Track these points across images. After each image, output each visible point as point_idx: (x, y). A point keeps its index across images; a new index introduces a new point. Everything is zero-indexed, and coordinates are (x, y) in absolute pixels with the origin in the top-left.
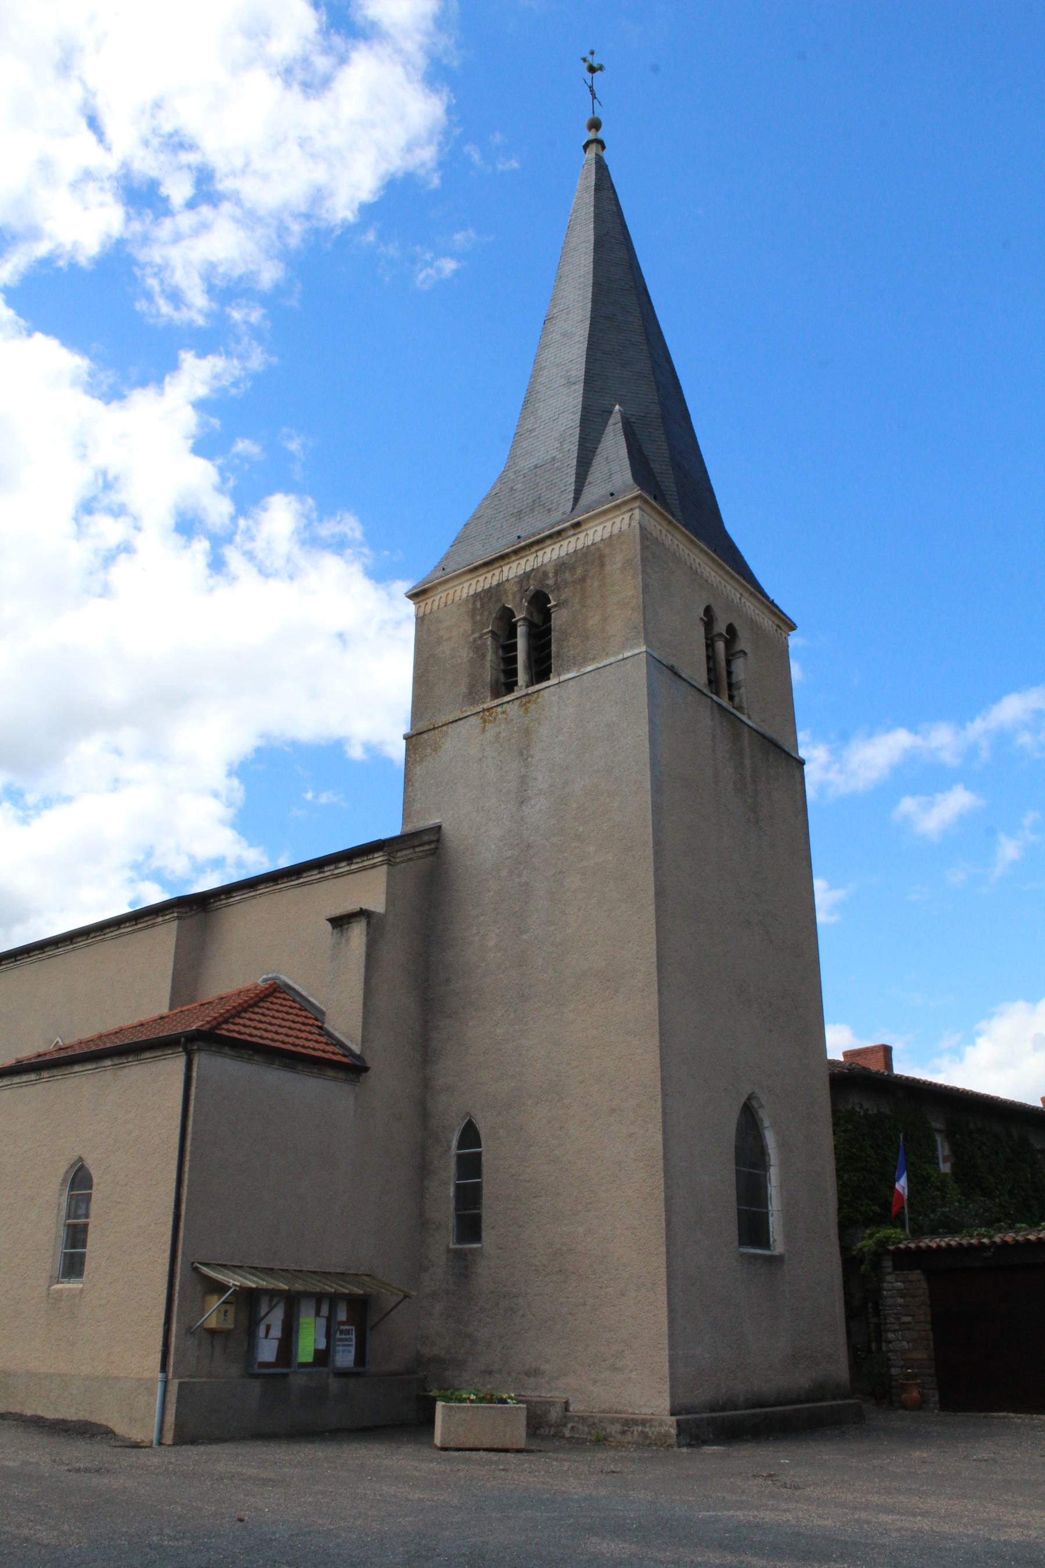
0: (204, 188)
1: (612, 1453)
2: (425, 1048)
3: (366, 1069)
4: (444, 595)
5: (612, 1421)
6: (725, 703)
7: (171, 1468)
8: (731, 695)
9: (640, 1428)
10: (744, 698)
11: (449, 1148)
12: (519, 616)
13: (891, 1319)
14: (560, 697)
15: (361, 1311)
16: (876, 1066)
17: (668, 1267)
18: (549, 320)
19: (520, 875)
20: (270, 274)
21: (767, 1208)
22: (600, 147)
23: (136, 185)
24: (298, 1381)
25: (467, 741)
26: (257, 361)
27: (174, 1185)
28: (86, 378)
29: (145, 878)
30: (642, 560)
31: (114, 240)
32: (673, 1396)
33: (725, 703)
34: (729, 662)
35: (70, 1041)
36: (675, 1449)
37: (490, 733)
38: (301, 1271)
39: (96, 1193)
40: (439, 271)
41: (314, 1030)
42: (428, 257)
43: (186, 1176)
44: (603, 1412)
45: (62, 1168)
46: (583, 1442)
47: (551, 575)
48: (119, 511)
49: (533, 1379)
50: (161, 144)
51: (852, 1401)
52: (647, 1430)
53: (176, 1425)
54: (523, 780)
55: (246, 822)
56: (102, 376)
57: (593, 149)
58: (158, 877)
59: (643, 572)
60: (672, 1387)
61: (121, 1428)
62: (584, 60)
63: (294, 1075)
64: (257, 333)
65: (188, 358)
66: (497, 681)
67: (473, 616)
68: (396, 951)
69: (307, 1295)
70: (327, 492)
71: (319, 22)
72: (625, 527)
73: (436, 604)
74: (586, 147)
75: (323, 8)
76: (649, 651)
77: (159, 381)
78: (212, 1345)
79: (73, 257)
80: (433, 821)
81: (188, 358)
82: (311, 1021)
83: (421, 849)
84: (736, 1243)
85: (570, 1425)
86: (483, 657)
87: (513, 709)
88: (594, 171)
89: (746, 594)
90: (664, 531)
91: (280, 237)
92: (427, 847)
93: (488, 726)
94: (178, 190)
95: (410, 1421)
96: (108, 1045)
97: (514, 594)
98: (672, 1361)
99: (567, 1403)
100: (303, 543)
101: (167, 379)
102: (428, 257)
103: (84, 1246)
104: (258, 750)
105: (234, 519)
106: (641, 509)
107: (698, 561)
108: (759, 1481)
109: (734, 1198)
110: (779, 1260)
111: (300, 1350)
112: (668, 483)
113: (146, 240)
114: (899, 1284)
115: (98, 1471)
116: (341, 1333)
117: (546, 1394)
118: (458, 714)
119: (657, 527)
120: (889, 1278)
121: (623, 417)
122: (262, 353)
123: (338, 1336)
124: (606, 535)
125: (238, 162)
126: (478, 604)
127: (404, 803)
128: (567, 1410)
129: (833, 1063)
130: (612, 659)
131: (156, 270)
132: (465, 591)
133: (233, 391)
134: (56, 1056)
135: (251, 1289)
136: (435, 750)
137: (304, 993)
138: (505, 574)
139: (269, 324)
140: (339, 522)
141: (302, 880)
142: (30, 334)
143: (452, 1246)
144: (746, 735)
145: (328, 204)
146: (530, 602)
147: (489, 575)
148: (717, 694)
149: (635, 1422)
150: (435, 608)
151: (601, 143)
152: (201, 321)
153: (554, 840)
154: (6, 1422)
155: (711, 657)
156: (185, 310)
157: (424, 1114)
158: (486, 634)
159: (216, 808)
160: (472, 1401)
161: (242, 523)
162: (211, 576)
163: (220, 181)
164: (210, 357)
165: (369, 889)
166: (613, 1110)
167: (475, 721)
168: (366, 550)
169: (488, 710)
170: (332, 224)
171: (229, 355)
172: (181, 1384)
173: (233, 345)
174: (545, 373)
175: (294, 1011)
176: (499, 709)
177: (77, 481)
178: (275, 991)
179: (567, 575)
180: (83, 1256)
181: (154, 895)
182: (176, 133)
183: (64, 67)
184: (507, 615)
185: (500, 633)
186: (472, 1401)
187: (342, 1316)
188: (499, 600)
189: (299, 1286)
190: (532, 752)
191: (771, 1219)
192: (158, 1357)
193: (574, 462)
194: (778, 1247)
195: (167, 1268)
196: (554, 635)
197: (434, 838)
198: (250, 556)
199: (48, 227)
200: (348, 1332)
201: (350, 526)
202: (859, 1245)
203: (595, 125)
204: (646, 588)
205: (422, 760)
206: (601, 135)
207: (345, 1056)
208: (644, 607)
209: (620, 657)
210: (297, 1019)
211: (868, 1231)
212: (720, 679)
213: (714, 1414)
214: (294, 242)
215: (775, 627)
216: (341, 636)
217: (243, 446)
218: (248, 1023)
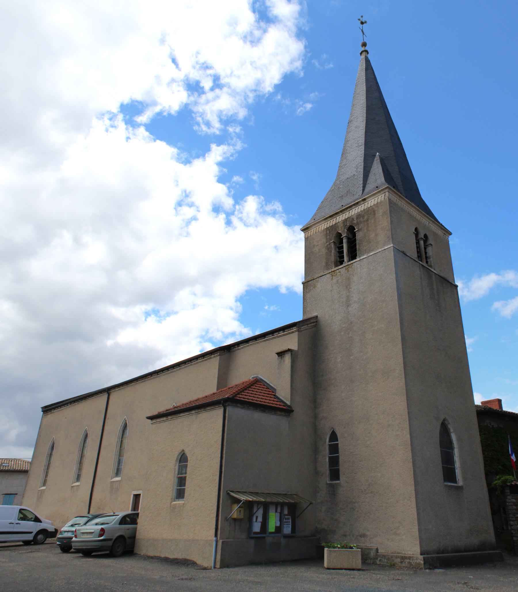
0: (217, 82)
1: (397, 571)
3: (293, 411)
4: (315, 229)
5: (397, 557)
6: (425, 264)
7: (219, 577)
8: (427, 262)
9: (408, 561)
11: (326, 442)
12: (344, 235)
13: (511, 516)
15: (292, 509)
16: (496, 407)
17: (415, 490)
18: (350, 122)
19: (348, 334)
20: (242, 113)
21: (454, 466)
23: (191, 83)
24: (269, 540)
26: (239, 146)
27: (219, 459)
28: (176, 156)
29: (206, 341)
31: (184, 104)
33: (425, 264)
34: (425, 249)
35: (179, 404)
36: (423, 570)
37: (335, 281)
38: (269, 493)
39: (189, 464)
40: (305, 108)
41: (272, 396)
42: (301, 103)
43: (224, 456)
44: (392, 553)
45: (176, 454)
48: (191, 205)
50: (200, 67)
51: (497, 551)
52: (411, 561)
54: (348, 297)
55: (243, 318)
56: (182, 155)
57: (364, 54)
58: (210, 340)
59: (390, 216)
60: (420, 542)
61: (199, 562)
62: (359, 20)
63: (265, 414)
64: (238, 136)
65: (214, 147)
66: (336, 260)
67: (326, 237)
69: (272, 503)
70: (268, 194)
71: (255, 18)
72: (383, 199)
73: (312, 232)
74: (361, 54)
75: (257, 13)
77: (204, 156)
78: (235, 525)
79: (169, 111)
80: (315, 314)
81: (214, 147)
82: (271, 393)
84: (443, 480)
85: (379, 559)
86: (331, 251)
87: (343, 271)
89: (431, 222)
90: (398, 200)
91: (245, 99)
92: (312, 324)
93: (334, 277)
94: (207, 84)
95: (314, 558)
96: (194, 405)
97: (341, 227)
98: (420, 531)
99: (377, 549)
100: (260, 213)
101: (207, 155)
102: (301, 103)
103: (185, 486)
104: (247, 291)
105: (234, 206)
106: (388, 192)
108: (461, 585)
109: (440, 462)
111: (270, 526)
112: (399, 182)
113: (196, 103)
114: (514, 500)
115: (190, 579)
116: (286, 519)
117: (368, 545)
118: (322, 274)
119: (395, 199)
120: (509, 497)
121: (380, 157)
123: (284, 520)
124: (376, 203)
125: (229, 72)
126: (328, 232)
127: (303, 308)
128: (377, 552)
129: (477, 406)
130: (380, 250)
132: (323, 227)
133: (231, 158)
135: (250, 501)
136: (314, 287)
137: (268, 382)
138: (338, 220)
139: (243, 132)
140: (273, 205)
142: (155, 141)
143: (328, 482)
144: (434, 277)
145: (262, 85)
146: (348, 230)
147: (332, 221)
148: (421, 261)
149: (406, 558)
150: (312, 234)
151: (367, 52)
152: (218, 132)
153: (361, 320)
154: (154, 560)
155: (418, 247)
156: (212, 128)
157: (315, 428)
159: (232, 314)
160: (339, 548)
161: (237, 207)
162: (227, 227)
165: (292, 342)
166: (389, 425)
167: (328, 276)
168: (283, 215)
169: (333, 271)
171: (229, 144)
172: (223, 542)
173: (230, 141)
174: (350, 142)
175: (265, 389)
177: (175, 195)
178: (257, 382)
179: (361, 219)
180: (184, 490)
181: (209, 347)
182: (205, 63)
183: (162, 41)
184: (339, 235)
186: (339, 548)
187: (286, 512)
189: (269, 500)
191: (456, 471)
192: (214, 530)
194: (460, 483)
195: (217, 493)
197: (315, 321)
198: (241, 219)
199: (159, 100)
200: (288, 519)
201: (277, 206)
202: (495, 483)
203: (364, 45)
205: (309, 291)
206: (367, 48)
207: (284, 406)
208: (391, 230)
209: (383, 249)
210: (265, 392)
211: (498, 477)
212: (422, 255)
214: (251, 101)
216: (276, 247)
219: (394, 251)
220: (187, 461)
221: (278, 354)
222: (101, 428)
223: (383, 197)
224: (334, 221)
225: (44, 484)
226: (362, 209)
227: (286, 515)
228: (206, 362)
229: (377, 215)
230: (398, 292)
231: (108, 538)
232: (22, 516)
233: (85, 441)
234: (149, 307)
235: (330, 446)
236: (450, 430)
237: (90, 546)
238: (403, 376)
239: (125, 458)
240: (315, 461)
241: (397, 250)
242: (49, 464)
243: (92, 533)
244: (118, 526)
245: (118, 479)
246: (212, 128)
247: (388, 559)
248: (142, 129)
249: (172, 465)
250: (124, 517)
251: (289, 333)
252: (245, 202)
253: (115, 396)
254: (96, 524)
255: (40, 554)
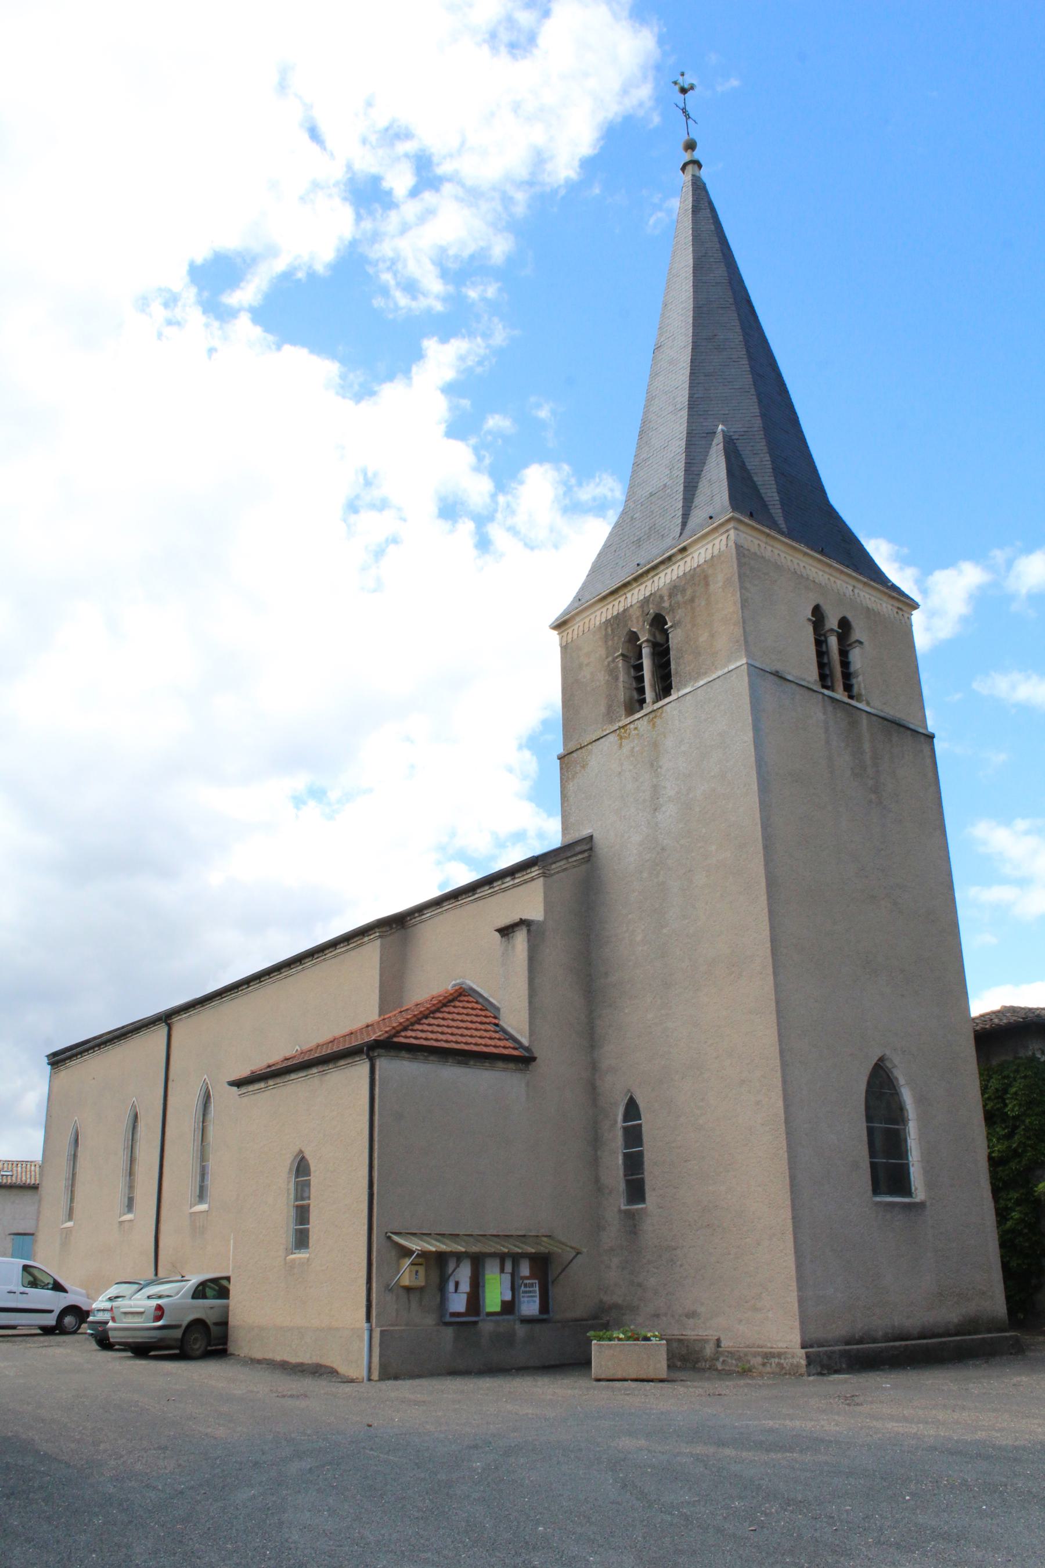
2: (590, 1036)
4: (581, 624)
5: (755, 1355)
6: (840, 695)
9: (777, 1360)
10: (862, 685)
11: (616, 1122)
14: (680, 711)
15: (543, 1265)
17: (793, 1218)
18: (658, 348)
20: (501, 248)
22: (696, 166)
24: (487, 1327)
25: (607, 757)
26: (500, 337)
28: (338, 380)
30: (740, 577)
31: (346, 243)
32: (803, 1331)
36: (805, 1378)
37: (626, 750)
39: (314, 1179)
44: (748, 1347)
45: (285, 1164)
46: (733, 1372)
47: (666, 598)
48: (382, 505)
49: (691, 1321)
52: (782, 1361)
53: (381, 1365)
54: (655, 788)
56: (351, 376)
58: (463, 857)
59: (742, 588)
61: (342, 1369)
62: (675, 83)
63: (467, 1070)
65: (431, 345)
66: (631, 698)
68: (557, 953)
72: (723, 548)
73: (576, 632)
76: (750, 662)
77: (407, 372)
78: (409, 1300)
79: (310, 267)
80: (585, 832)
81: (431, 345)
83: (574, 859)
84: (870, 1193)
86: (617, 679)
87: (643, 725)
88: (691, 193)
89: (860, 586)
90: (763, 545)
92: (580, 856)
94: (400, 181)
95: (576, 1362)
98: (801, 1301)
99: (718, 1341)
101: (414, 369)
105: (493, 496)
106: (736, 529)
107: (802, 564)
110: (922, 1205)
112: (770, 493)
113: (376, 237)
116: (526, 1285)
119: (756, 541)
122: (504, 328)
123: (523, 1288)
126: (609, 630)
130: (720, 673)
131: (388, 264)
132: (598, 619)
134: (284, 1065)
136: (583, 767)
137: (486, 995)
140: (598, 485)
141: (477, 896)
142: (279, 348)
143: (623, 1207)
145: (549, 167)
146: (651, 625)
147: (616, 603)
149: (773, 1355)
150: (575, 637)
151: (698, 164)
152: (439, 307)
155: (821, 653)
156: (421, 298)
157: (593, 1091)
158: (617, 657)
160: (620, 1339)
161: (501, 499)
163: (438, 165)
164: (452, 341)
165: (529, 902)
167: (613, 738)
169: (623, 727)
170: (556, 186)
171: (471, 335)
172: (382, 1332)
176: (632, 726)
179: (679, 598)
180: (308, 1230)
184: (633, 637)
185: (630, 655)
186: (620, 1339)
187: (525, 1270)
188: (626, 625)
190: (661, 763)
191: (912, 1170)
192: (364, 1310)
193: (681, 488)
194: (919, 1191)
196: (673, 654)
197: (585, 847)
198: (513, 530)
200: (532, 1285)
203: (690, 146)
204: (744, 603)
205: (573, 777)
206: (697, 155)
207: (515, 1049)
208: (744, 622)
209: (726, 670)
213: (847, 1347)
214: (520, 210)
215: (896, 610)
217: (495, 422)
218: (442, 1022)
219: (749, 675)
220: (308, 1173)
221: (499, 931)
222: (162, 1101)
223: (724, 542)
224: (622, 605)
225: (70, 1216)
226: (681, 574)
227: (527, 1278)
228: (353, 953)
229: (712, 587)
230: (759, 773)
231: (173, 1323)
232: (31, 1279)
233: (134, 1128)
234: (300, 782)
235: (626, 1130)
236: (897, 1079)
237: (140, 1338)
238: (770, 970)
239: (211, 1164)
240: (595, 1162)
241: (756, 672)
242: (74, 1175)
243: (142, 1313)
244: (190, 1300)
245: (203, 1207)
246: (421, 298)
247: (739, 1359)
248: (244, 321)
249: (283, 1182)
250: (203, 1284)
251: (526, 882)
252: (522, 483)
253: (182, 1027)
254: (149, 1297)
255: (59, 1351)
